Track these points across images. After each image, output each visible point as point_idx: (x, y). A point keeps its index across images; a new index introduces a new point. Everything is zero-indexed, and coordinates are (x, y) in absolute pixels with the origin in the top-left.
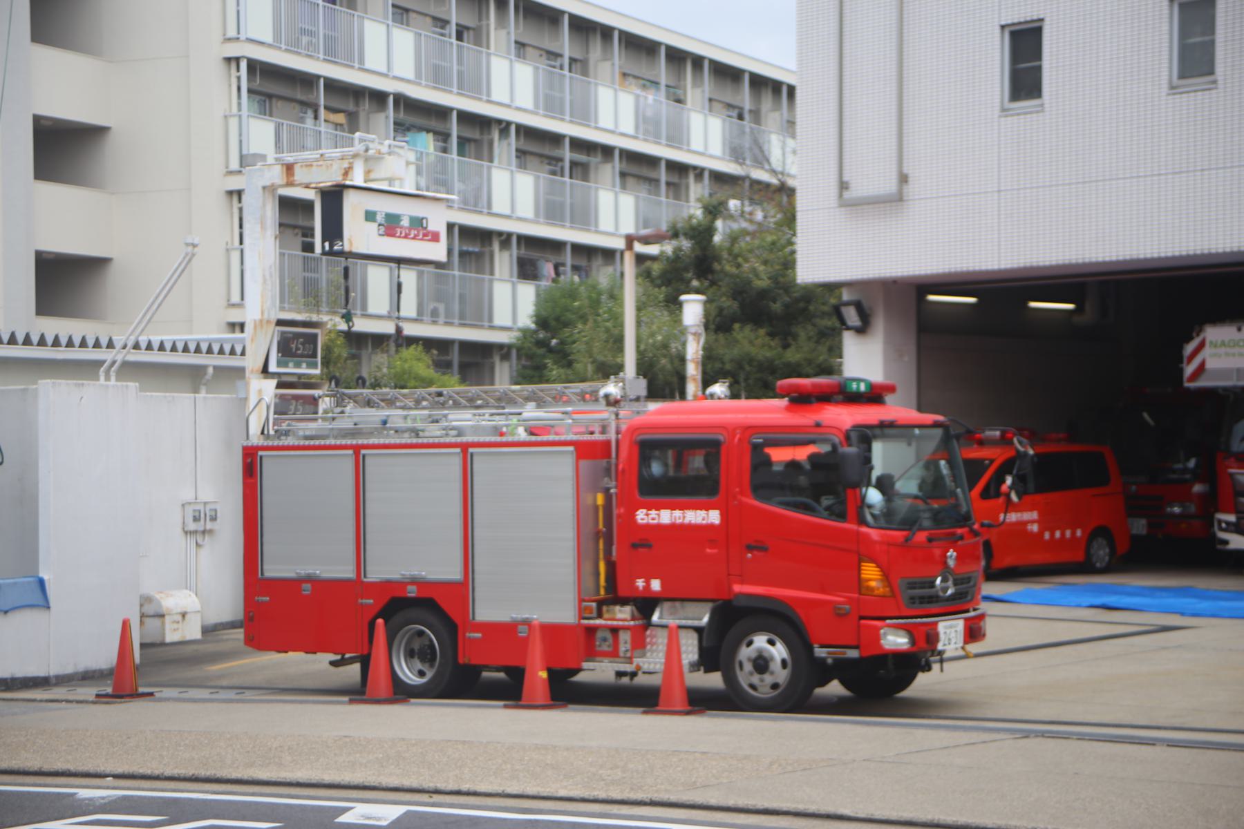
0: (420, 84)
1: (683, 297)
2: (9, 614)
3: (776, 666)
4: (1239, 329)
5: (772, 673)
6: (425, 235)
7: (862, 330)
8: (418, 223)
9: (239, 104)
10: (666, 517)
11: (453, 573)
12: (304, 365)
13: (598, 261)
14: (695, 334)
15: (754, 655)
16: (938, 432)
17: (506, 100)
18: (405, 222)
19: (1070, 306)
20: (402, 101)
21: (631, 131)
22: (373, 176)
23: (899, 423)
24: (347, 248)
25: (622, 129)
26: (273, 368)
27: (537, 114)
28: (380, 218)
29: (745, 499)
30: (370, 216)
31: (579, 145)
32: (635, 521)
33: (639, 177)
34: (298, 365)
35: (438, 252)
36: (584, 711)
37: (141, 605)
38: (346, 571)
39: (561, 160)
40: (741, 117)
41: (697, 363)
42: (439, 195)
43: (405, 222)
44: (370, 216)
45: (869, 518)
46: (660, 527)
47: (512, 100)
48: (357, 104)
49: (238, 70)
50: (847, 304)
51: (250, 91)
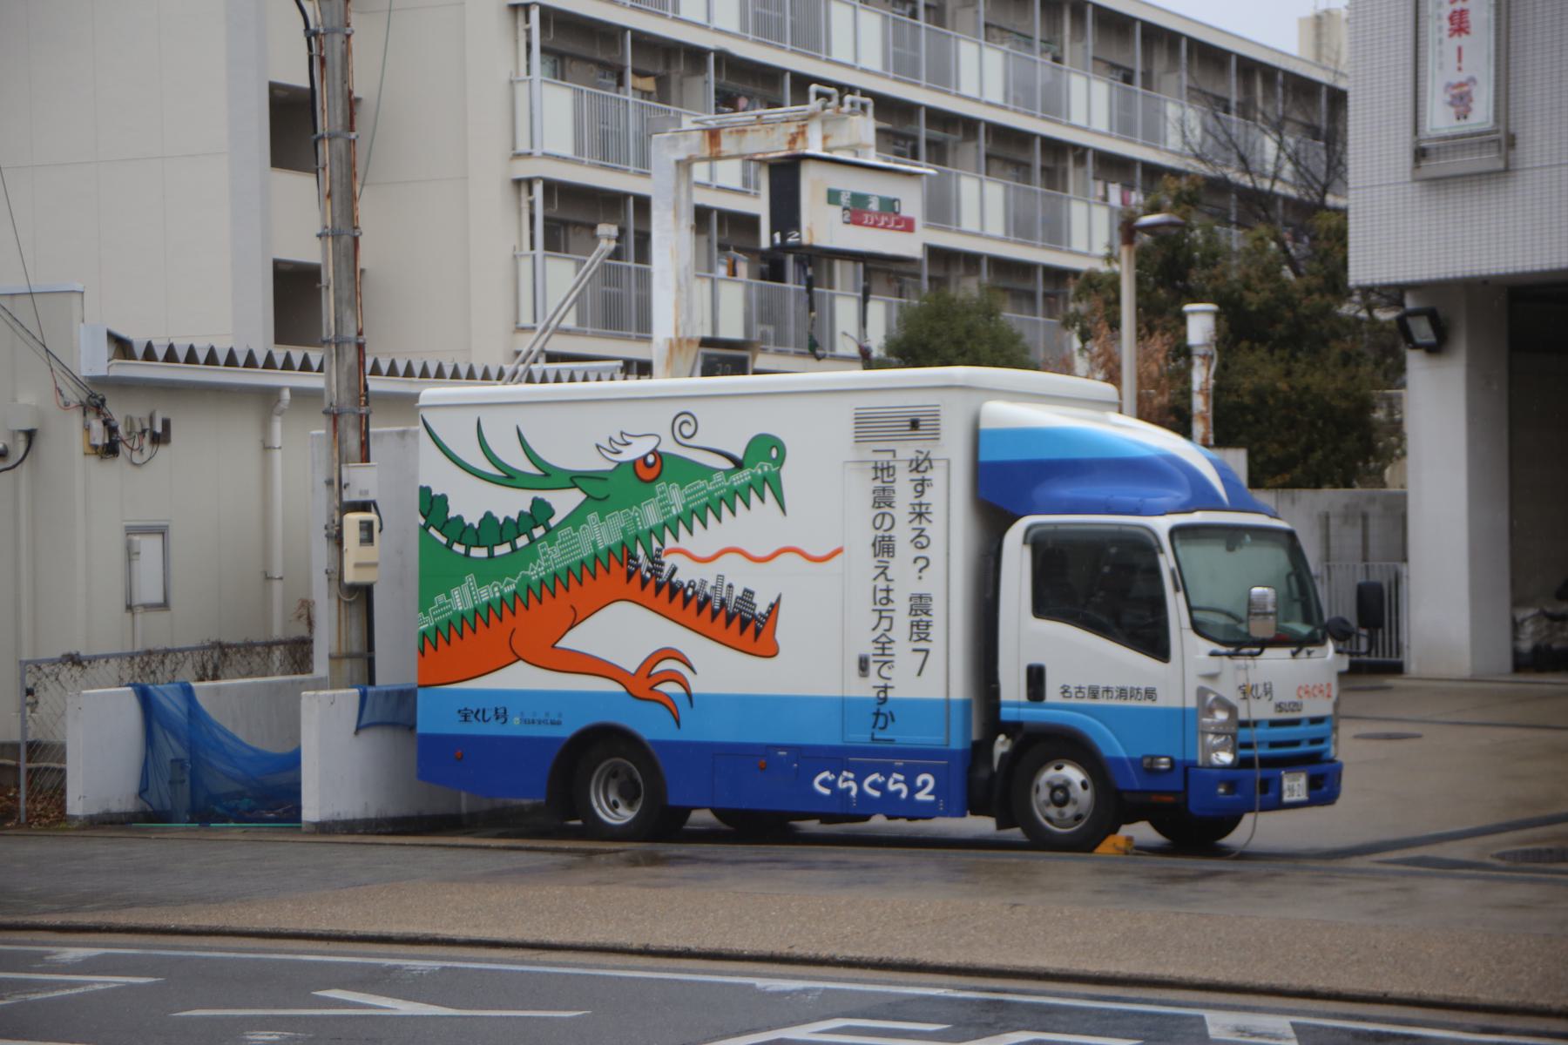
0: (746, 39)
1: (1188, 307)
5: (1075, 802)
6: (897, 223)
8: (889, 205)
9: (528, 67)
13: (958, 271)
14: (1204, 357)
17: (849, 60)
18: (874, 206)
20: (727, 61)
21: (999, 100)
22: (831, 143)
24: (806, 240)
25: (988, 97)
27: (886, 77)
28: (844, 199)
30: (833, 197)
31: (940, 118)
33: (1007, 161)
39: (915, 139)
40: (1128, 78)
41: (1207, 396)
43: (874, 206)
47: (856, 59)
48: (667, 66)
49: (527, 20)
50: (1416, 313)
51: (543, 50)
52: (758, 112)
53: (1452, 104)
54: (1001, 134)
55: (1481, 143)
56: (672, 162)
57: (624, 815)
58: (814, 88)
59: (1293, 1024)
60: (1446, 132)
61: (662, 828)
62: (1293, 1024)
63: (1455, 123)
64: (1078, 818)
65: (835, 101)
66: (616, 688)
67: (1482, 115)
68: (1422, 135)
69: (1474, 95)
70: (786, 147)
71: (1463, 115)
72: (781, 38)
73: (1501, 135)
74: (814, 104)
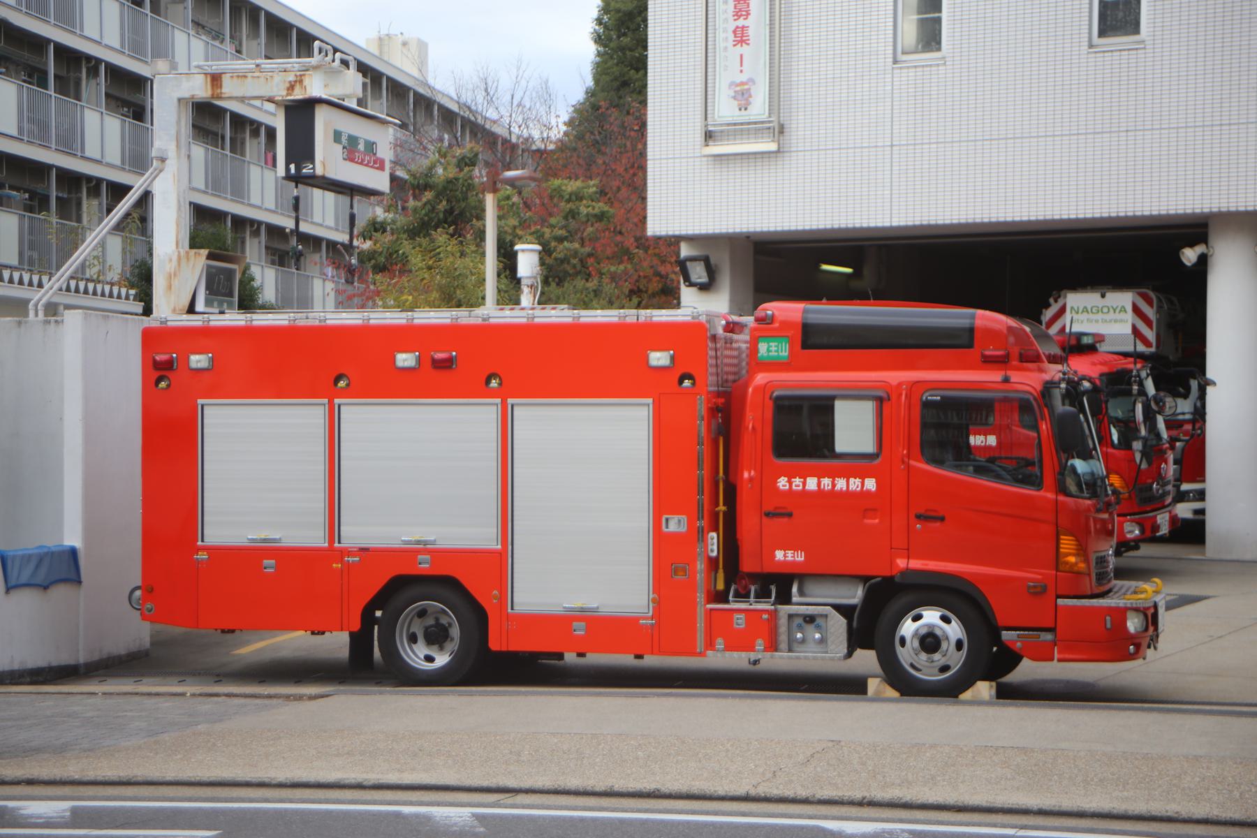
2: (49, 591)
3: (948, 646)
4: (1103, 296)
11: (483, 536)
15: (916, 644)
19: (849, 270)
24: (319, 172)
29: (912, 463)
36: (840, 700)
37: (1136, 610)
38: (315, 537)
45: (1073, 489)
46: (805, 493)
52: (258, 61)
53: (734, 98)
55: (755, 129)
56: (175, 101)
58: (317, 43)
60: (730, 120)
63: (737, 112)
65: (330, 57)
67: (759, 108)
68: (710, 121)
70: (284, 93)
73: (775, 124)
74: (316, 59)
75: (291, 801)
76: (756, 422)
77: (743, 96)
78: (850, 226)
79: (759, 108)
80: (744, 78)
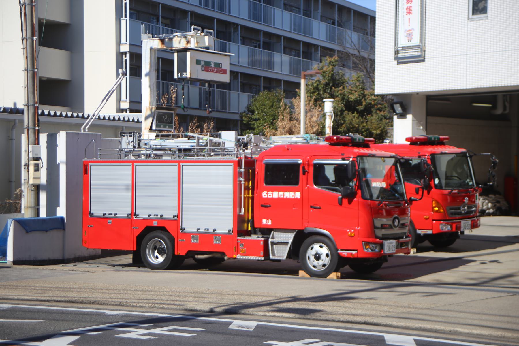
1: (324, 100)
3: (323, 257)
6: (220, 71)
7: (402, 116)
8: (218, 65)
10: (276, 195)
12: (167, 127)
16: (393, 160)
23: (377, 155)
26: (154, 128)
28: (202, 63)
30: (198, 62)
32: (262, 197)
34: (165, 127)
35: (225, 78)
42: (227, 54)
44: (198, 62)
46: (273, 199)
53: (406, 36)
54: (288, 40)
57: (161, 259)
59: (415, 340)
61: (175, 263)
62: (415, 340)
64: (324, 265)
66: (249, 225)
67: (416, 41)
69: (413, 34)
71: (410, 40)
72: (214, 8)
75: (147, 312)
76: (260, 170)
77: (409, 35)
78: (503, 85)
79: (416, 41)
80: (410, 28)
